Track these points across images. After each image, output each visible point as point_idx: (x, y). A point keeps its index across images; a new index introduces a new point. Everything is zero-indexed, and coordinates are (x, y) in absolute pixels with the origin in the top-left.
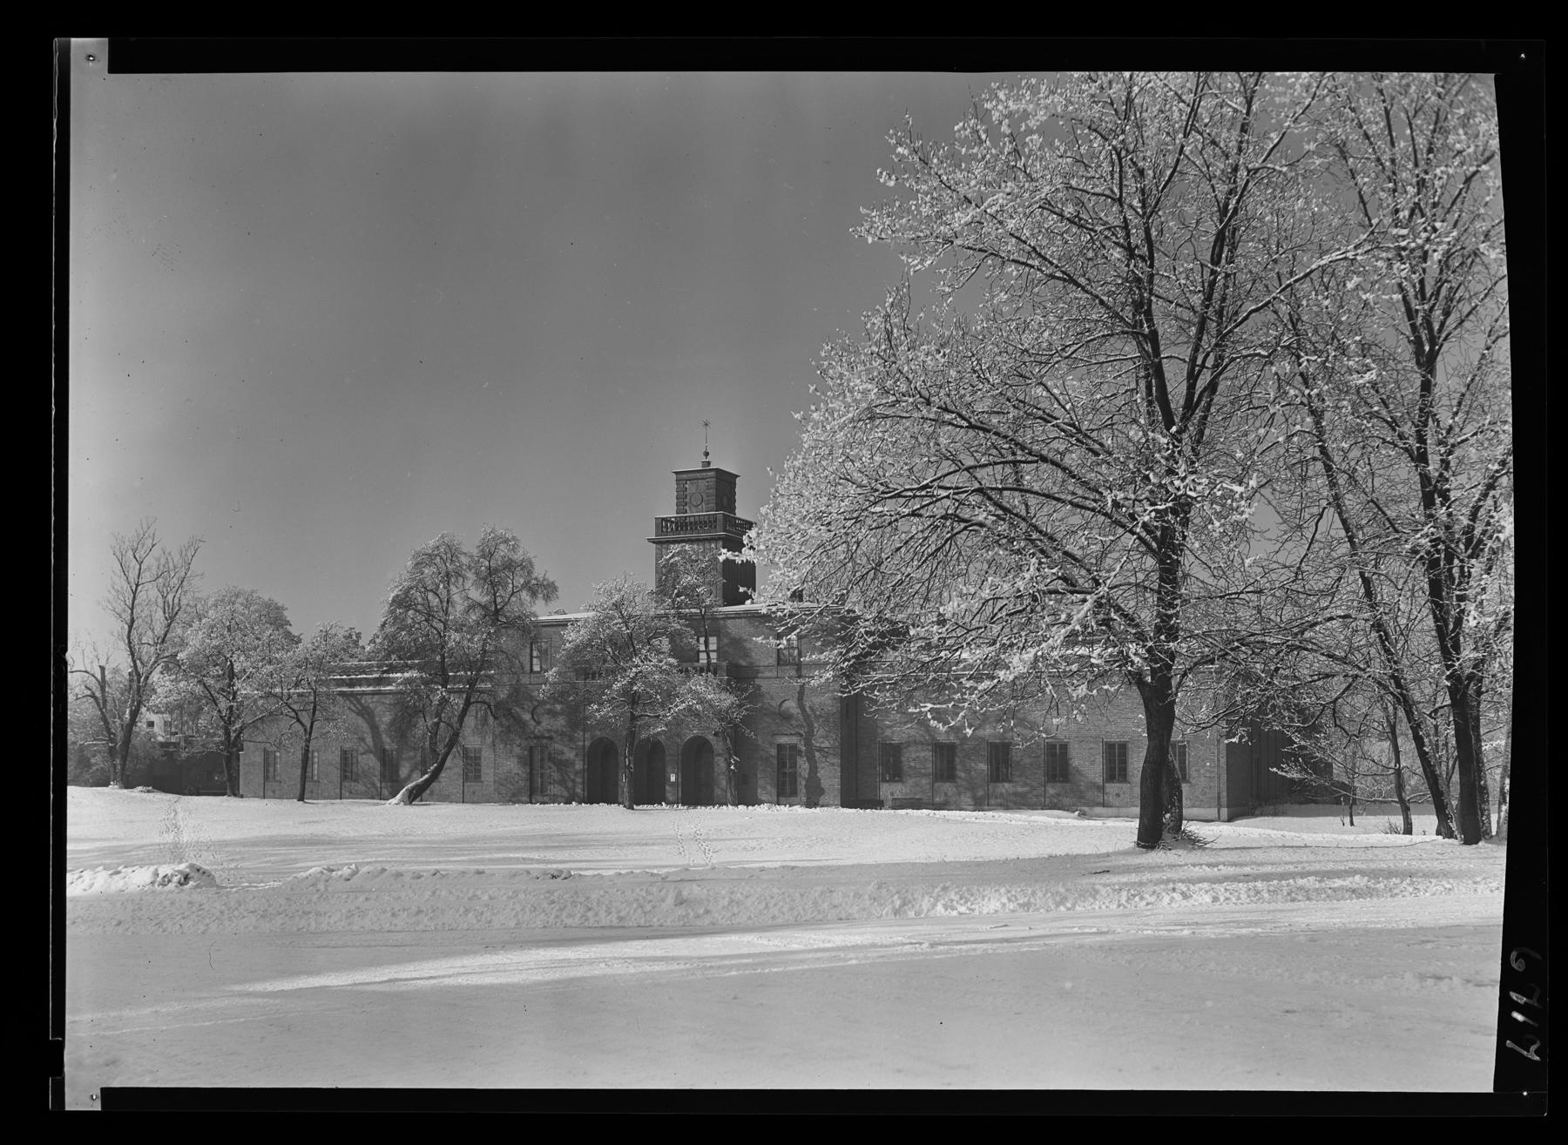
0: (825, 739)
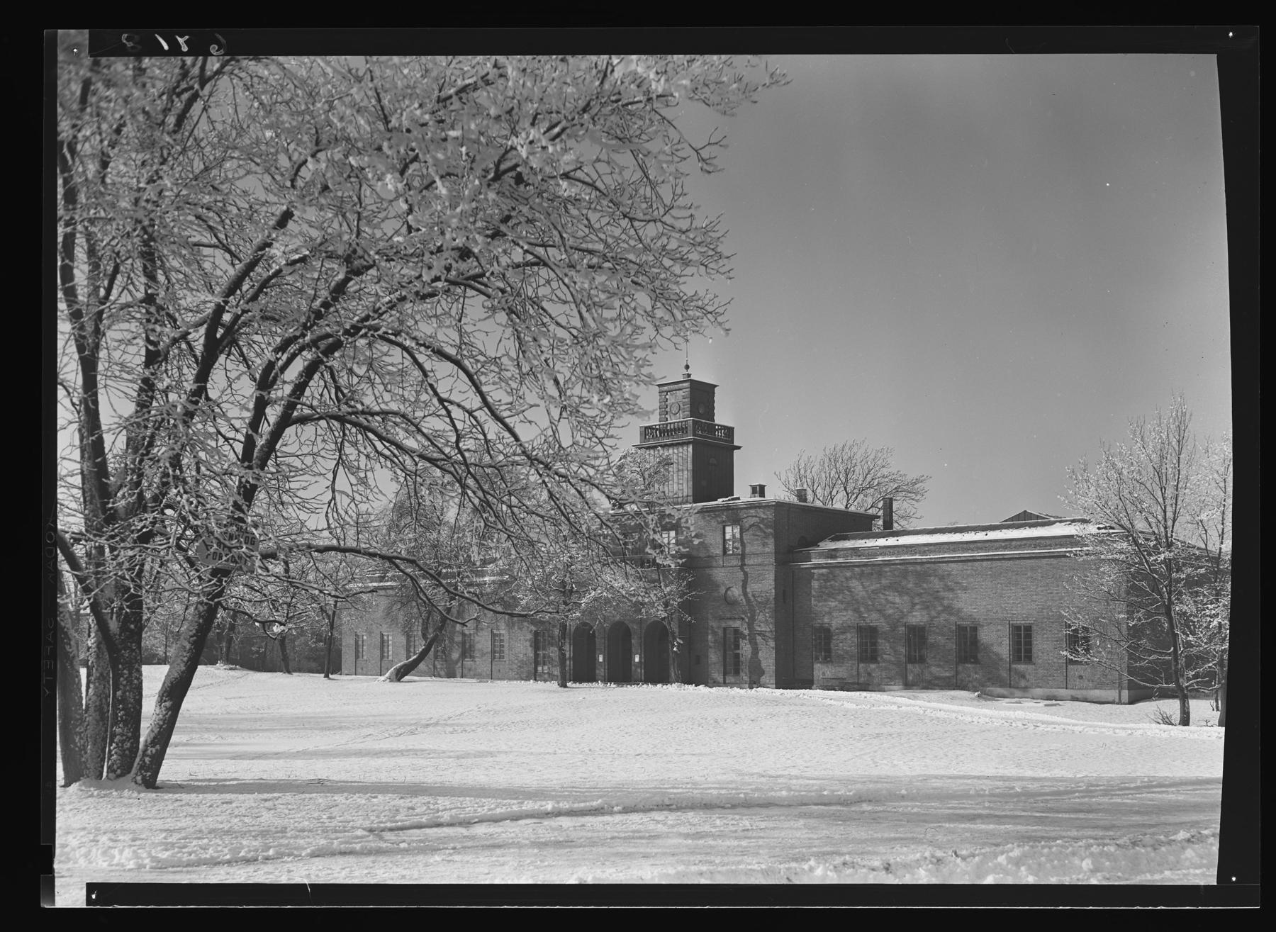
0: (765, 623)
